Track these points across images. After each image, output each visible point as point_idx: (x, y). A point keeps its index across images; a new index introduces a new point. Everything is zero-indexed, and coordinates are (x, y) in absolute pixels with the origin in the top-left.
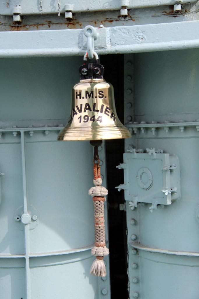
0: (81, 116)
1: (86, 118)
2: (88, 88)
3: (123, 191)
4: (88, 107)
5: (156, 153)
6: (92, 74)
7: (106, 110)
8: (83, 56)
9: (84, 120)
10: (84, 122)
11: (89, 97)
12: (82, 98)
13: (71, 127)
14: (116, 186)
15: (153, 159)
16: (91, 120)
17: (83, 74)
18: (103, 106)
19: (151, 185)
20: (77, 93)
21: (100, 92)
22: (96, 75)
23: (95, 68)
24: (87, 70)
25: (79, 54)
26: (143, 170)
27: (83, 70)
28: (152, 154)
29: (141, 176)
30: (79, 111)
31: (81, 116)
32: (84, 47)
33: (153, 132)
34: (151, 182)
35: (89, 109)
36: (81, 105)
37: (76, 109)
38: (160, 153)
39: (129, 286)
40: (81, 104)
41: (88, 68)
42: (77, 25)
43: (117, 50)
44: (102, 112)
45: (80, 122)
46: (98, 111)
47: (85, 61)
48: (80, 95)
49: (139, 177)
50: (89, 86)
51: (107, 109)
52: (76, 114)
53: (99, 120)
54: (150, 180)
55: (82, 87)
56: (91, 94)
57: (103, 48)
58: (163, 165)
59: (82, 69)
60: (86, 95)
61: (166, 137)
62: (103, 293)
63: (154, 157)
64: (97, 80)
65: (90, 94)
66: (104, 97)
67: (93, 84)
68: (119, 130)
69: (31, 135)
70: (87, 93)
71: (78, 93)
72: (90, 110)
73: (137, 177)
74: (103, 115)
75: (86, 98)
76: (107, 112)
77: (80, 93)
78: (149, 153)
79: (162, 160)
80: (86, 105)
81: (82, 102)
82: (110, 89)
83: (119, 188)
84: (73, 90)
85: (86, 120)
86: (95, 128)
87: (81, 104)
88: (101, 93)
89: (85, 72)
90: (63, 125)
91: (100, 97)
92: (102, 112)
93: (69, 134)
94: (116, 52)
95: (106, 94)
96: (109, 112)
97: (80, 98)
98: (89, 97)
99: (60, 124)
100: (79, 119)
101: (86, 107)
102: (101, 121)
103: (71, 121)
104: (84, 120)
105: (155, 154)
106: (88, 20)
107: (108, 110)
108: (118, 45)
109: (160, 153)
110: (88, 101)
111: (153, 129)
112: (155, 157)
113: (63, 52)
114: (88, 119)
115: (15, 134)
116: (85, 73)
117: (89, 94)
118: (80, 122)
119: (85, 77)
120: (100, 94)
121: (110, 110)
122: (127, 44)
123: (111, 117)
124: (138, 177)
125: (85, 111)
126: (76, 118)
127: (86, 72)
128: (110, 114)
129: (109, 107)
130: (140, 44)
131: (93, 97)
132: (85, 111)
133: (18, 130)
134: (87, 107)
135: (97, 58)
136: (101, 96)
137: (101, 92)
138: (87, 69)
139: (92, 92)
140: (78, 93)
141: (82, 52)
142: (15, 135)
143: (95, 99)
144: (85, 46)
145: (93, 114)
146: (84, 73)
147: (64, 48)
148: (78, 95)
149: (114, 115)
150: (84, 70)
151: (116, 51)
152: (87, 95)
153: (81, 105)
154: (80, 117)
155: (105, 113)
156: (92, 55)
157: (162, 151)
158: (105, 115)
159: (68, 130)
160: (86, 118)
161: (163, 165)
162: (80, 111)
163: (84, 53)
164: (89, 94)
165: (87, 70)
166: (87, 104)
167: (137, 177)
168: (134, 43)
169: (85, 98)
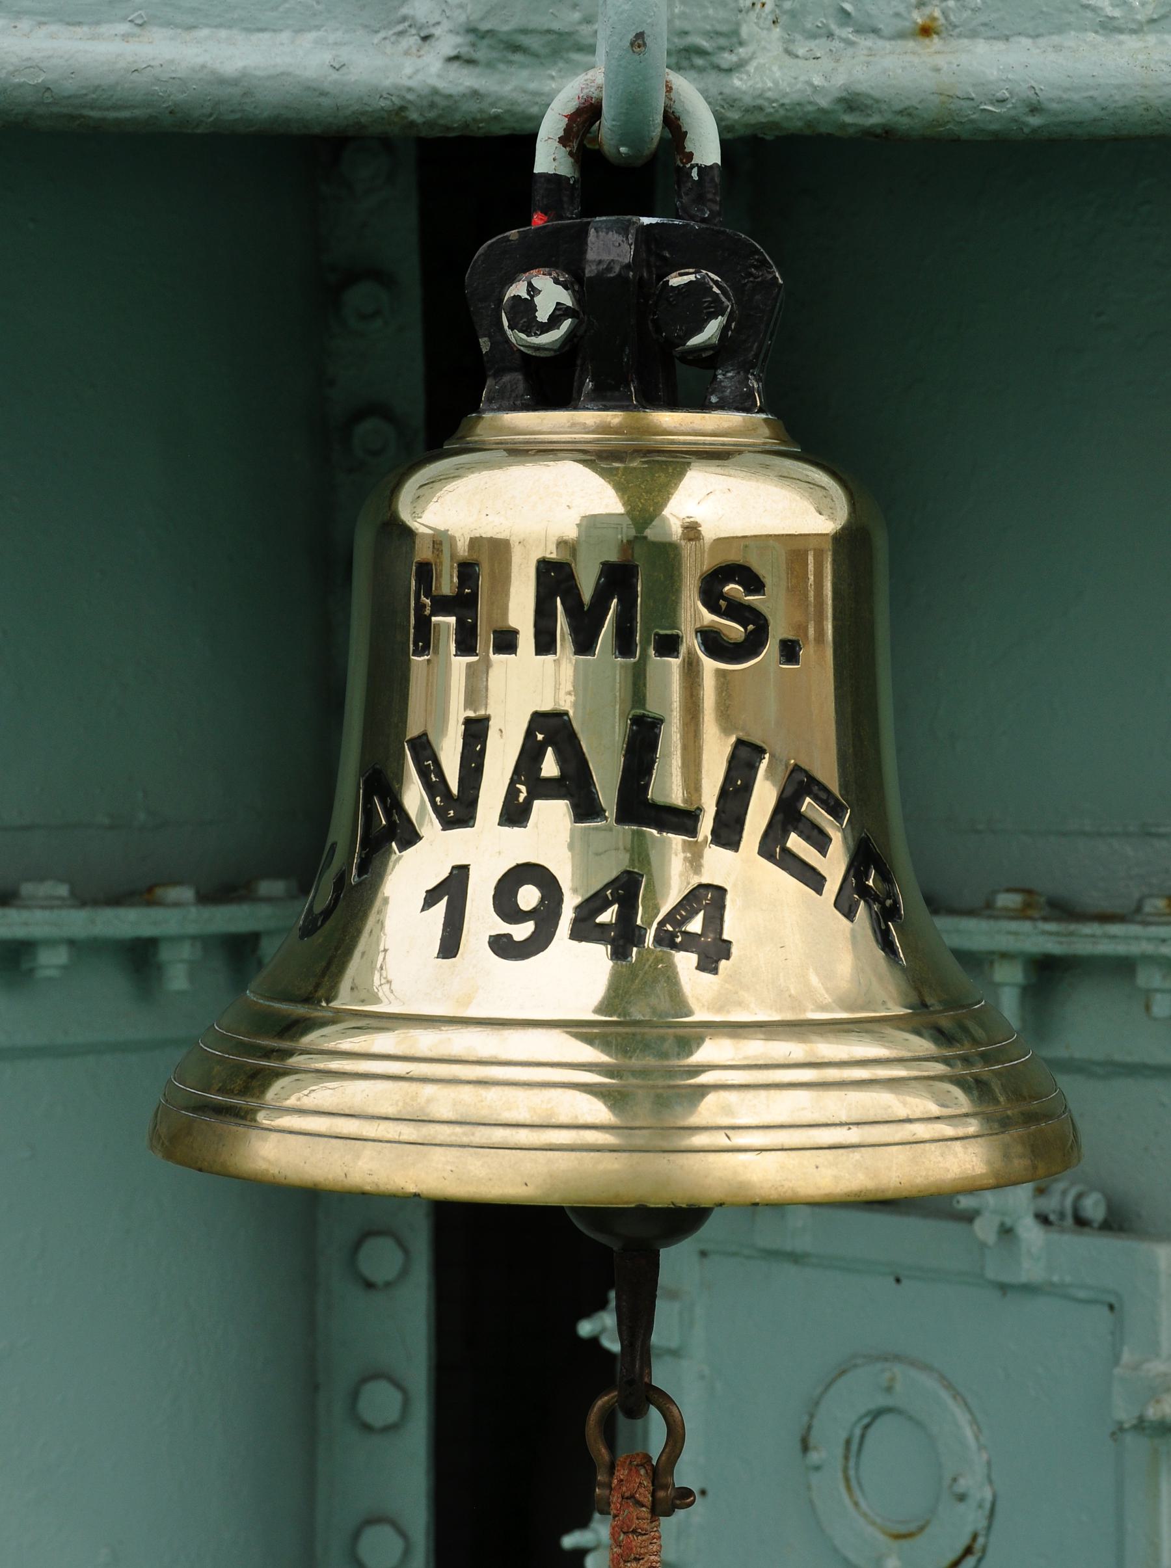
0: (460, 873)
1: (528, 897)
2: (591, 524)
4: (555, 756)
5: (1043, 1219)
6: (626, 357)
7: (786, 816)
8: (527, 142)
9: (504, 928)
10: (503, 947)
11: (584, 645)
12: (485, 639)
13: (343, 1001)
14: (568, 1530)
15: (1004, 1288)
16: (584, 929)
17: (517, 337)
19: (968, 1551)
20: (425, 572)
22: (681, 370)
23: (675, 281)
24: (566, 298)
25: (414, 116)
26: (889, 1389)
27: (519, 289)
28: (1007, 1231)
29: (852, 1449)
30: (440, 812)
31: (460, 873)
32: (472, 30)
34: (971, 1519)
36: (476, 732)
37: (414, 797)
38: (1081, 1222)
41: (590, 271)
43: (862, 88)
45: (450, 946)
46: (682, 820)
47: (554, 180)
48: (463, 603)
49: (827, 1452)
51: (797, 797)
52: (410, 837)
53: (690, 942)
54: (962, 1498)
55: (518, 497)
57: (701, 52)
58: (1136, 1367)
59: (511, 280)
61: (1135, 1058)
63: (1026, 1264)
65: (607, 597)
66: (771, 649)
67: (646, 470)
68: (958, 1082)
70: (554, 578)
71: (447, 584)
72: (586, 809)
73: (805, 1447)
74: (739, 869)
75: (545, 644)
76: (795, 842)
78: (978, 1224)
79: (1111, 1307)
80: (530, 734)
85: (522, 931)
86: (642, 1048)
88: (732, 588)
89: (543, 316)
90: (63, 890)
92: (728, 832)
93: (323, 1095)
94: (848, 119)
95: (799, 608)
96: (821, 842)
97: (624, 644)
99: (42, 879)
100: (441, 906)
102: (713, 953)
103: (339, 920)
104: (504, 928)
105: (1030, 1233)
106: (137, 112)
107: (808, 805)
108: (875, 31)
109: (1081, 1222)
110: (581, 686)
112: (1030, 1270)
113: (222, 81)
114: (546, 916)
116: (545, 328)
117: (587, 594)
118: (450, 946)
119: (550, 384)
120: (711, 596)
121: (835, 810)
122: (973, 34)
124: (814, 1457)
126: (409, 876)
127: (560, 314)
128: (834, 865)
130: (1131, 42)
132: (515, 814)
134: (550, 767)
135: (707, 150)
136: (734, 630)
137: (733, 576)
138: (575, 280)
140: (447, 584)
141: (441, 85)
143: (460, 664)
144: (485, 26)
145: (640, 852)
146: (532, 326)
147: (223, 33)
148: (443, 605)
149: (885, 876)
150: (532, 290)
151: (851, 102)
154: (452, 888)
156: (659, 119)
157: (1094, 1208)
160: (528, 897)
161: (1136, 1367)
162: (458, 810)
163: (535, 110)
164: (587, 594)
165: (566, 298)
166: (550, 729)
167: (805, 1447)
168: (1060, 29)
169: (526, 640)
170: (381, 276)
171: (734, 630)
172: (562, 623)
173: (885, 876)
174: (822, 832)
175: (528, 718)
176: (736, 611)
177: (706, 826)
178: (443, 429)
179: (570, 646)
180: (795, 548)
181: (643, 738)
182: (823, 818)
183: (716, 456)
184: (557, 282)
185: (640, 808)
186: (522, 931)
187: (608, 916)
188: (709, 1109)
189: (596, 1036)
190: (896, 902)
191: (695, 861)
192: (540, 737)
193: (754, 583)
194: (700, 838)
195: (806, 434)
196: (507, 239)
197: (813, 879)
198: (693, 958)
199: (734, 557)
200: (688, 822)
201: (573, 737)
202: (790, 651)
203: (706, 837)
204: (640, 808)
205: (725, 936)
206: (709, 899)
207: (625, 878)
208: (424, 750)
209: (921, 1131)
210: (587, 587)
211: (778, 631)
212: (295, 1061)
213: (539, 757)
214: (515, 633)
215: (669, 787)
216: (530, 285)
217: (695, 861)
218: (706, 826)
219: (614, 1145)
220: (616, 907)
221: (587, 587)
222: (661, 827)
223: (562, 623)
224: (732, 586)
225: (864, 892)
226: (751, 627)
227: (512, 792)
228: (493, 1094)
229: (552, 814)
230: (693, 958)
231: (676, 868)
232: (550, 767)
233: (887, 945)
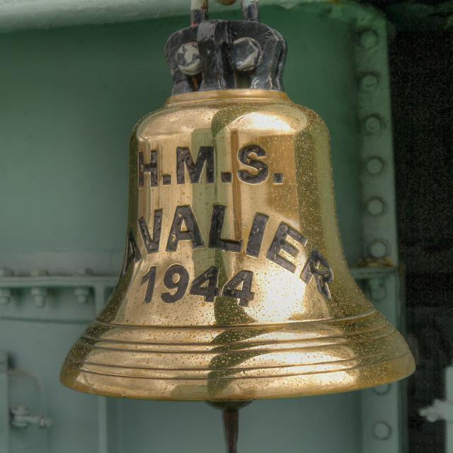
3: (441, 424)
11: (195, 180)
12: (218, 178)
16: (196, 290)
18: (260, 220)
20: (141, 156)
21: (249, 148)
36: (158, 214)
46: (236, 244)
50: (208, 116)
55: (177, 126)
56: (201, 159)
60: (179, 167)
65: (200, 161)
67: (229, 111)
70: (183, 153)
71: (148, 160)
72: (197, 242)
75: (181, 180)
81: (173, 195)
82: (304, 136)
83: (431, 413)
84: (134, 140)
85: (173, 292)
86: (235, 337)
88: (253, 154)
91: (249, 178)
96: (294, 251)
97: (210, 177)
101: (177, 223)
114: (182, 286)
115: (81, 295)
118: (148, 299)
119: (195, 82)
121: (301, 240)
125: (171, 247)
128: (301, 261)
129: (295, 225)
131: (210, 177)
132: (171, 247)
133: (87, 281)
134: (183, 227)
136: (253, 170)
139: (208, 153)
142: (82, 299)
145: (219, 260)
148: (148, 167)
149: (324, 264)
152: (205, 163)
159: (103, 337)
160: (177, 278)
169: (174, 179)
170: (375, 74)
171: (253, 170)
173: (324, 264)
174: (294, 248)
175: (175, 209)
176: (253, 162)
177: (244, 247)
178: (156, 102)
179: (189, 181)
180: (283, 137)
181: (218, 214)
182: (296, 243)
184: (193, 46)
185: (216, 240)
186: (173, 292)
187: (205, 284)
189: (261, 332)
190: (330, 275)
191: (240, 259)
192: (180, 216)
193: (261, 152)
194: (242, 252)
195: (297, 96)
196: (178, 34)
197: (291, 267)
199: (258, 143)
200: (238, 246)
201: (192, 215)
203: (244, 252)
204: (216, 240)
206: (247, 277)
207: (212, 269)
208: (142, 221)
209: (331, 367)
212: (97, 345)
213: (179, 223)
214: (170, 176)
215: (229, 232)
216: (184, 48)
217: (240, 259)
218: (244, 247)
220: (208, 281)
222: (227, 249)
224: (253, 153)
225: (313, 271)
226: (260, 169)
227: (170, 238)
229: (185, 247)
231: (232, 262)
232: (183, 227)
233: (324, 291)
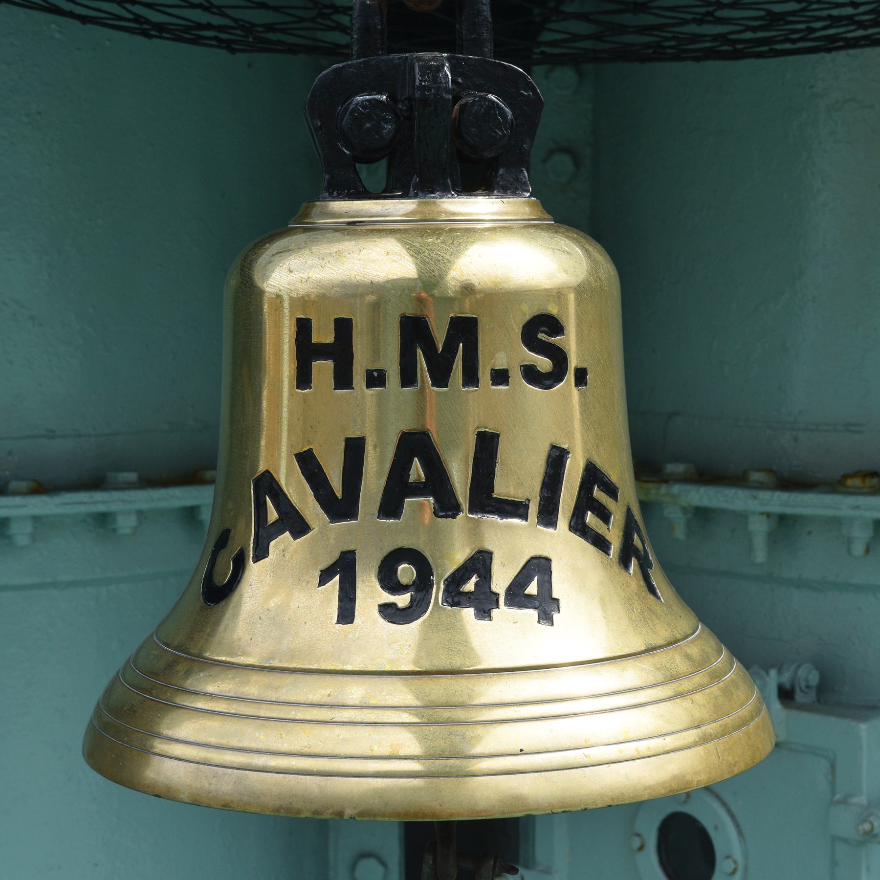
9: (387, 598)
10: (389, 612)
33: (760, 542)
35: (437, 484)
36: (354, 450)
39: (249, 23)
40: (348, 441)
42: (298, 299)
44: (548, 516)
45: (346, 614)
62: (372, 863)
64: (481, 207)
66: (570, 376)
69: (21, 540)
74: (560, 544)
75: (408, 378)
76: (590, 518)
77: (344, 327)
85: (403, 600)
87: (348, 441)
92: (548, 516)
96: (604, 515)
97: (343, 380)
98: (441, 378)
104: (387, 598)
111: (759, 528)
114: (423, 585)
118: (346, 614)
123: (624, 562)
125: (390, 507)
128: (614, 535)
132: (390, 507)
134: (417, 471)
136: (544, 363)
148: (323, 352)
153: (354, 450)
155: (579, 527)
158: (577, 540)
160: (406, 572)
166: (415, 445)
169: (533, 510)
171: (544, 363)
172: (422, 362)
183: (503, 227)
186: (403, 600)
188: (160, 746)
195: (565, 211)
197: (601, 543)
198: (471, 611)
202: (581, 377)
205: (555, 596)
206: (539, 566)
210: (440, 337)
211: (573, 363)
219: (417, 772)
221: (440, 337)
223: (422, 362)
228: (326, 732)
230: (471, 611)
